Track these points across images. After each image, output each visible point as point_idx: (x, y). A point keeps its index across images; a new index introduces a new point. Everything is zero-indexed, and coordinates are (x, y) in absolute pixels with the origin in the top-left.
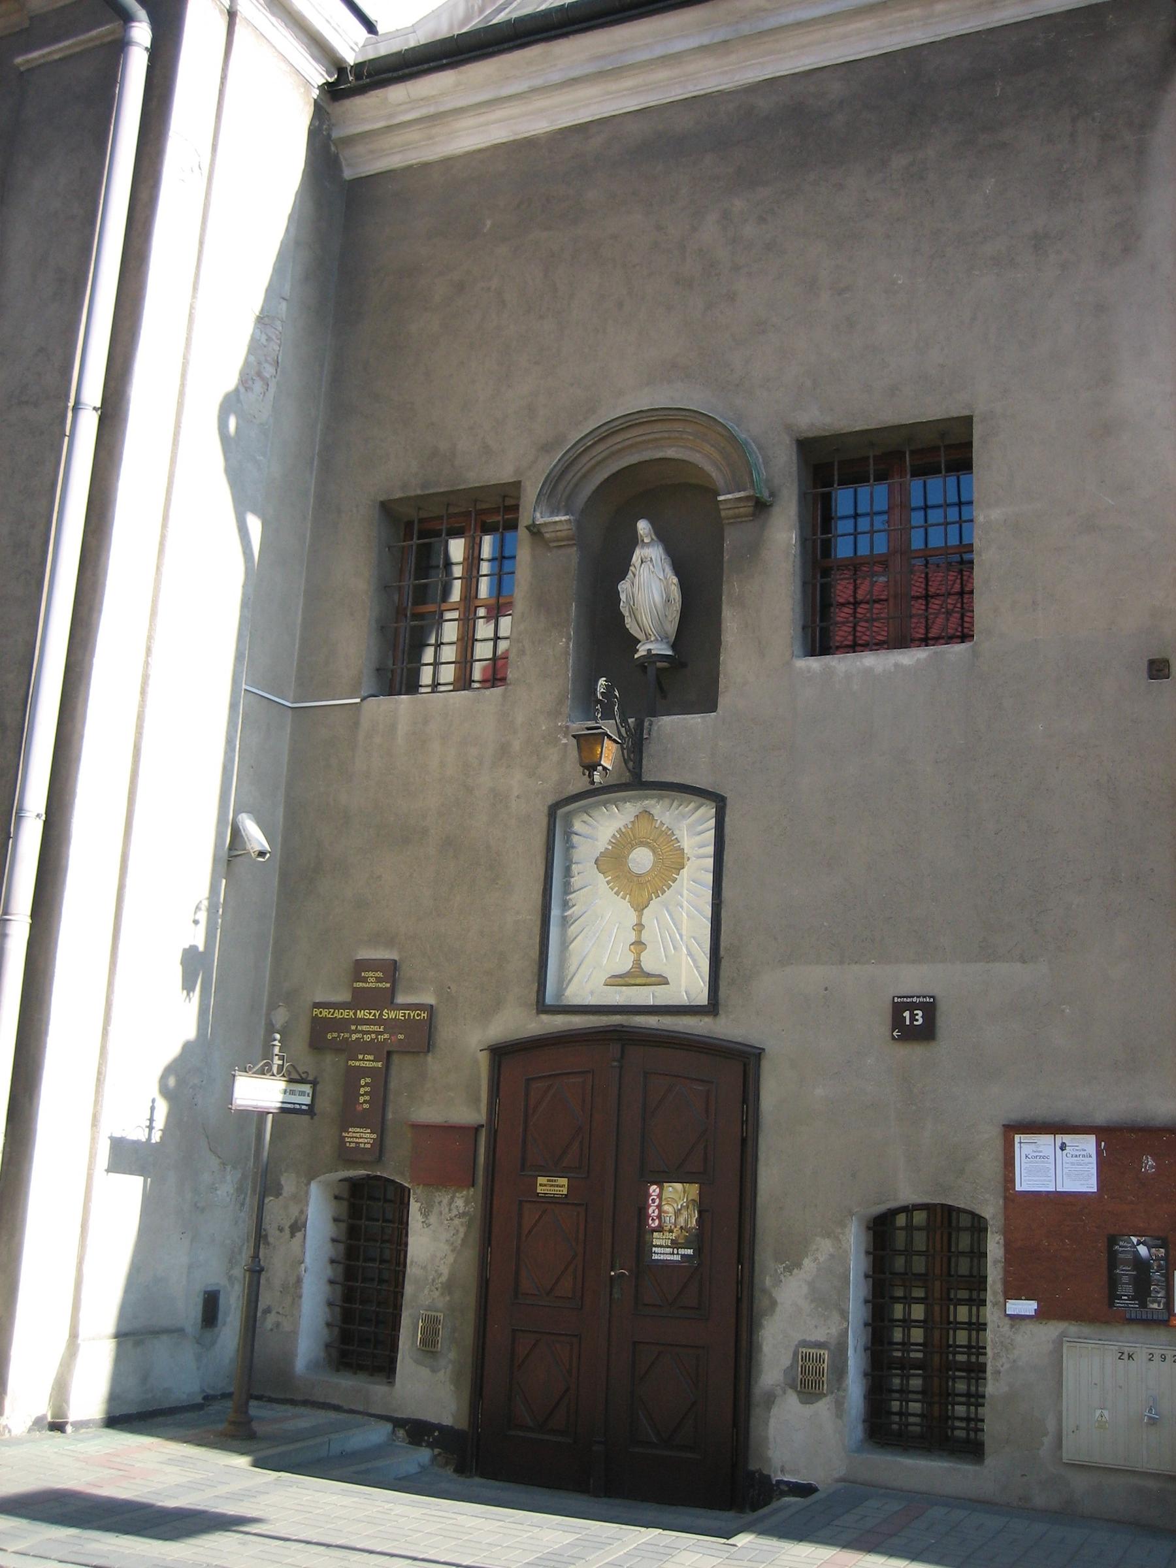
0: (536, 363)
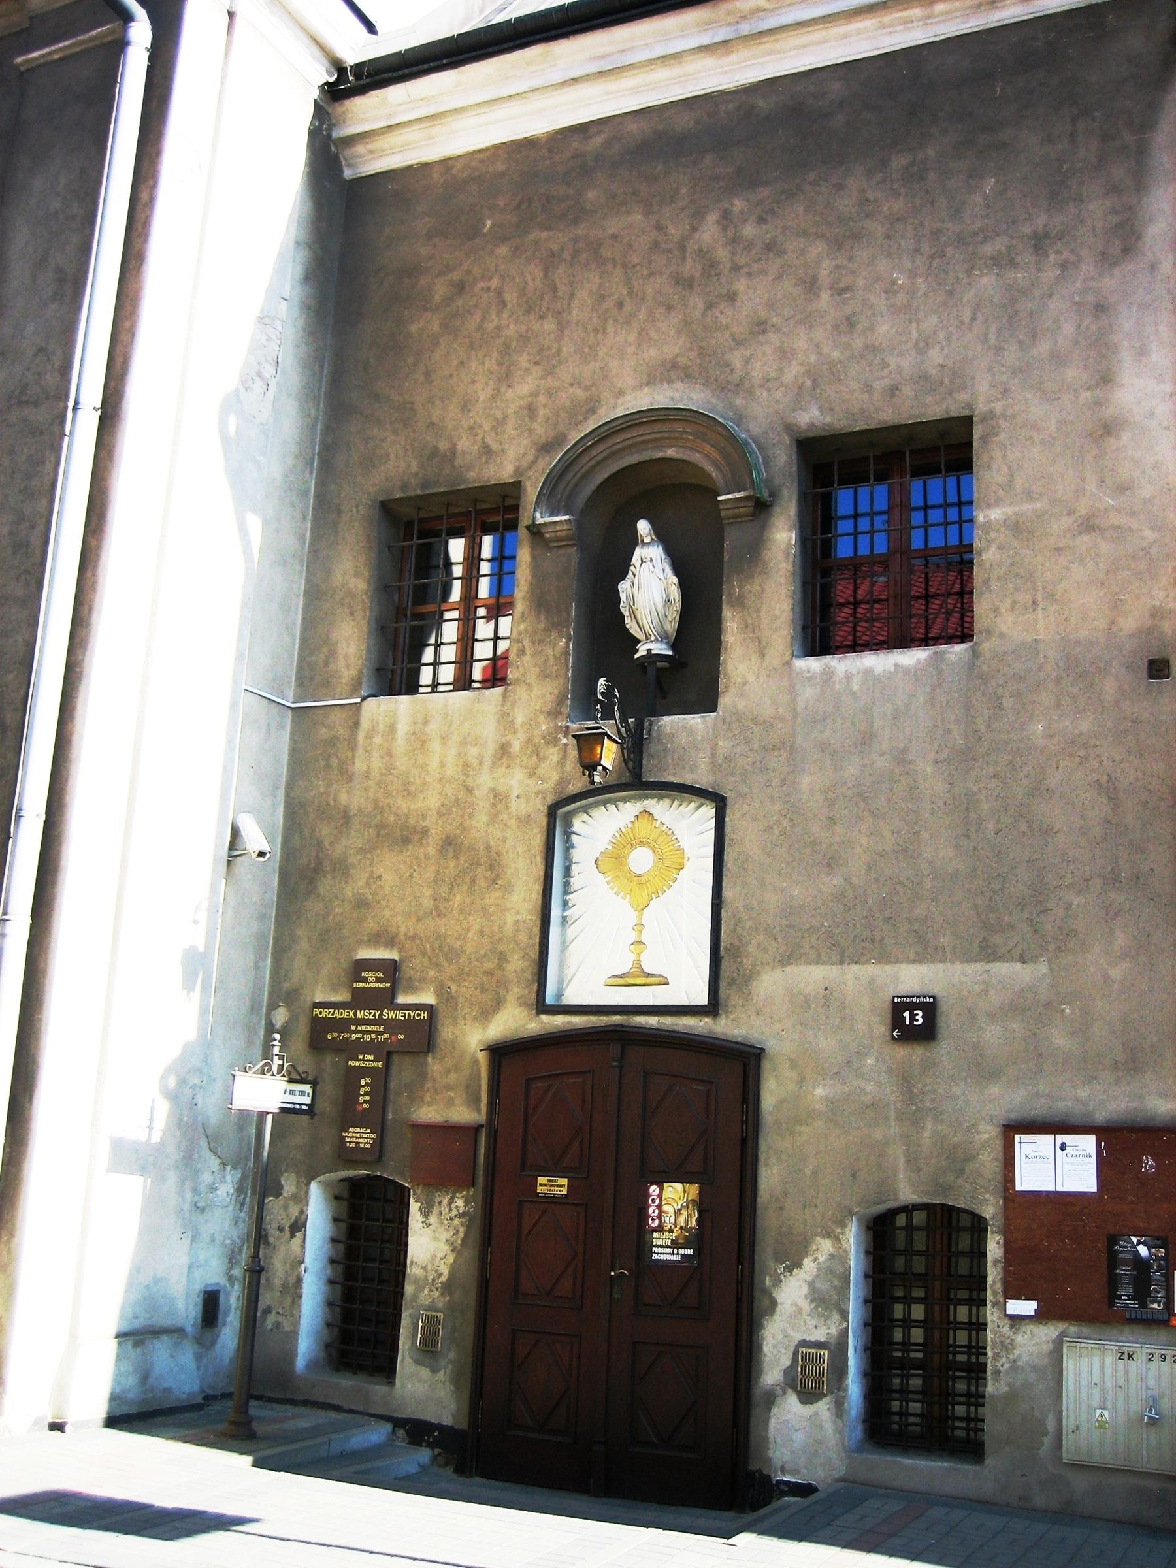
0: (536, 363)
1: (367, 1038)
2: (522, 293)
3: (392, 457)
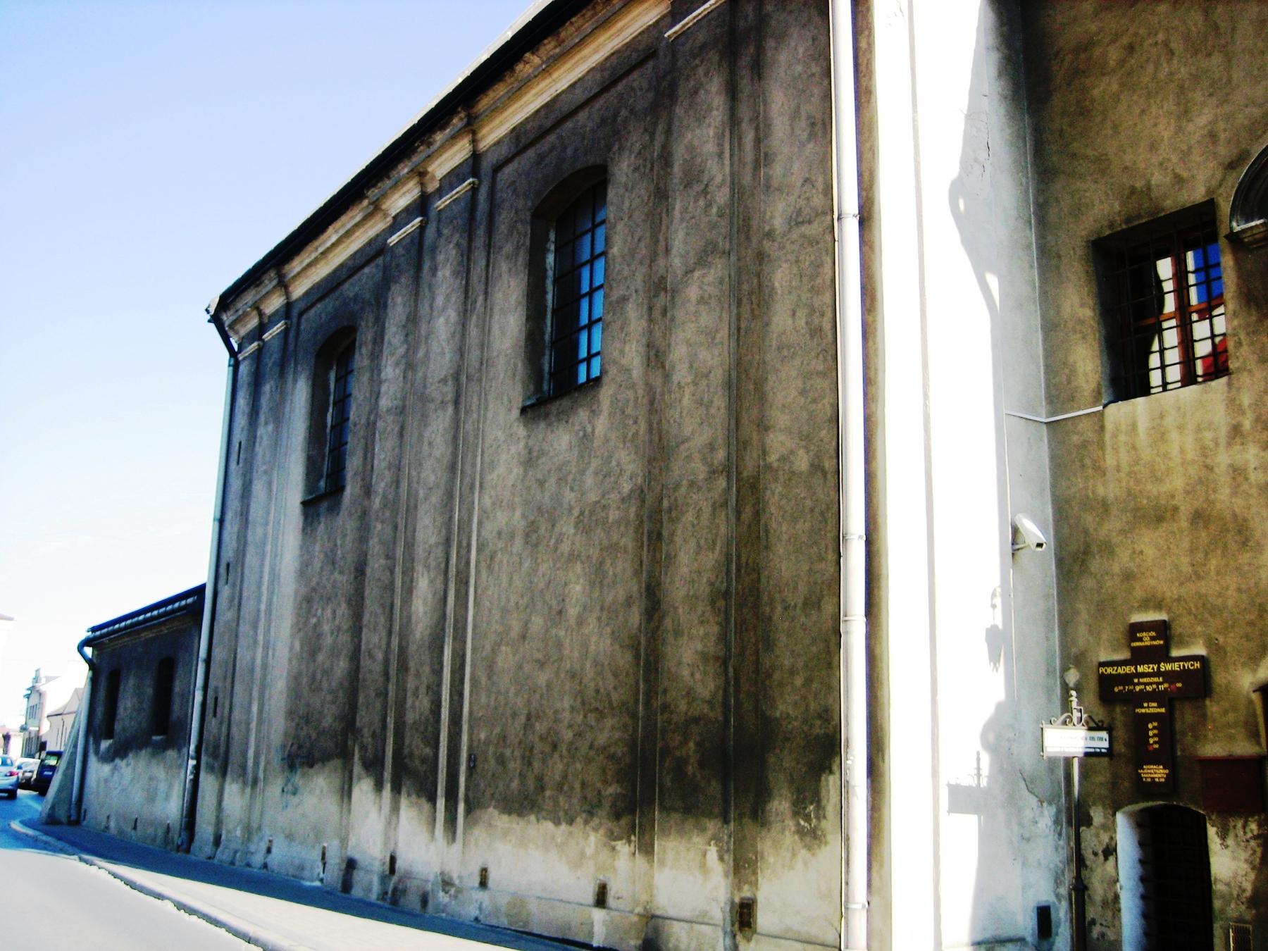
0: (1211, 95)
1: (1149, 688)
2: (1187, 37)
3: (1096, 202)
